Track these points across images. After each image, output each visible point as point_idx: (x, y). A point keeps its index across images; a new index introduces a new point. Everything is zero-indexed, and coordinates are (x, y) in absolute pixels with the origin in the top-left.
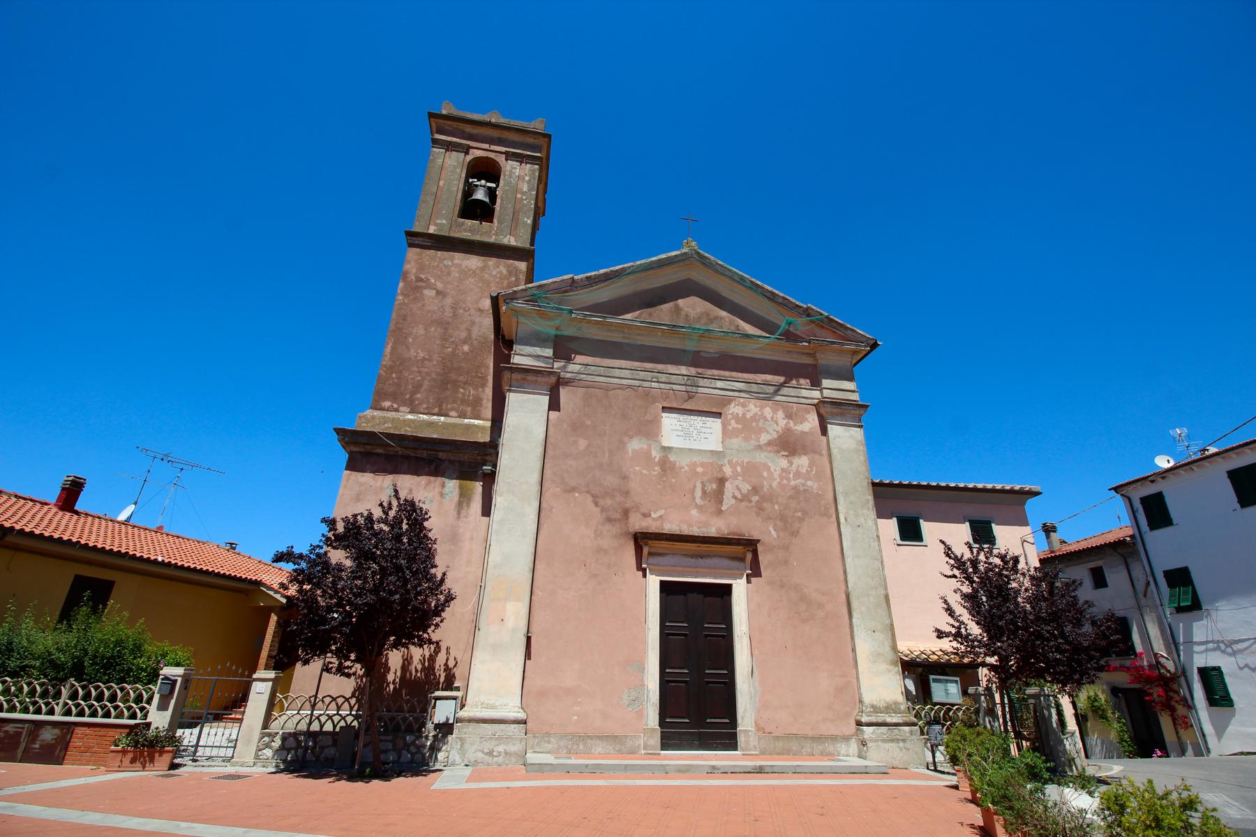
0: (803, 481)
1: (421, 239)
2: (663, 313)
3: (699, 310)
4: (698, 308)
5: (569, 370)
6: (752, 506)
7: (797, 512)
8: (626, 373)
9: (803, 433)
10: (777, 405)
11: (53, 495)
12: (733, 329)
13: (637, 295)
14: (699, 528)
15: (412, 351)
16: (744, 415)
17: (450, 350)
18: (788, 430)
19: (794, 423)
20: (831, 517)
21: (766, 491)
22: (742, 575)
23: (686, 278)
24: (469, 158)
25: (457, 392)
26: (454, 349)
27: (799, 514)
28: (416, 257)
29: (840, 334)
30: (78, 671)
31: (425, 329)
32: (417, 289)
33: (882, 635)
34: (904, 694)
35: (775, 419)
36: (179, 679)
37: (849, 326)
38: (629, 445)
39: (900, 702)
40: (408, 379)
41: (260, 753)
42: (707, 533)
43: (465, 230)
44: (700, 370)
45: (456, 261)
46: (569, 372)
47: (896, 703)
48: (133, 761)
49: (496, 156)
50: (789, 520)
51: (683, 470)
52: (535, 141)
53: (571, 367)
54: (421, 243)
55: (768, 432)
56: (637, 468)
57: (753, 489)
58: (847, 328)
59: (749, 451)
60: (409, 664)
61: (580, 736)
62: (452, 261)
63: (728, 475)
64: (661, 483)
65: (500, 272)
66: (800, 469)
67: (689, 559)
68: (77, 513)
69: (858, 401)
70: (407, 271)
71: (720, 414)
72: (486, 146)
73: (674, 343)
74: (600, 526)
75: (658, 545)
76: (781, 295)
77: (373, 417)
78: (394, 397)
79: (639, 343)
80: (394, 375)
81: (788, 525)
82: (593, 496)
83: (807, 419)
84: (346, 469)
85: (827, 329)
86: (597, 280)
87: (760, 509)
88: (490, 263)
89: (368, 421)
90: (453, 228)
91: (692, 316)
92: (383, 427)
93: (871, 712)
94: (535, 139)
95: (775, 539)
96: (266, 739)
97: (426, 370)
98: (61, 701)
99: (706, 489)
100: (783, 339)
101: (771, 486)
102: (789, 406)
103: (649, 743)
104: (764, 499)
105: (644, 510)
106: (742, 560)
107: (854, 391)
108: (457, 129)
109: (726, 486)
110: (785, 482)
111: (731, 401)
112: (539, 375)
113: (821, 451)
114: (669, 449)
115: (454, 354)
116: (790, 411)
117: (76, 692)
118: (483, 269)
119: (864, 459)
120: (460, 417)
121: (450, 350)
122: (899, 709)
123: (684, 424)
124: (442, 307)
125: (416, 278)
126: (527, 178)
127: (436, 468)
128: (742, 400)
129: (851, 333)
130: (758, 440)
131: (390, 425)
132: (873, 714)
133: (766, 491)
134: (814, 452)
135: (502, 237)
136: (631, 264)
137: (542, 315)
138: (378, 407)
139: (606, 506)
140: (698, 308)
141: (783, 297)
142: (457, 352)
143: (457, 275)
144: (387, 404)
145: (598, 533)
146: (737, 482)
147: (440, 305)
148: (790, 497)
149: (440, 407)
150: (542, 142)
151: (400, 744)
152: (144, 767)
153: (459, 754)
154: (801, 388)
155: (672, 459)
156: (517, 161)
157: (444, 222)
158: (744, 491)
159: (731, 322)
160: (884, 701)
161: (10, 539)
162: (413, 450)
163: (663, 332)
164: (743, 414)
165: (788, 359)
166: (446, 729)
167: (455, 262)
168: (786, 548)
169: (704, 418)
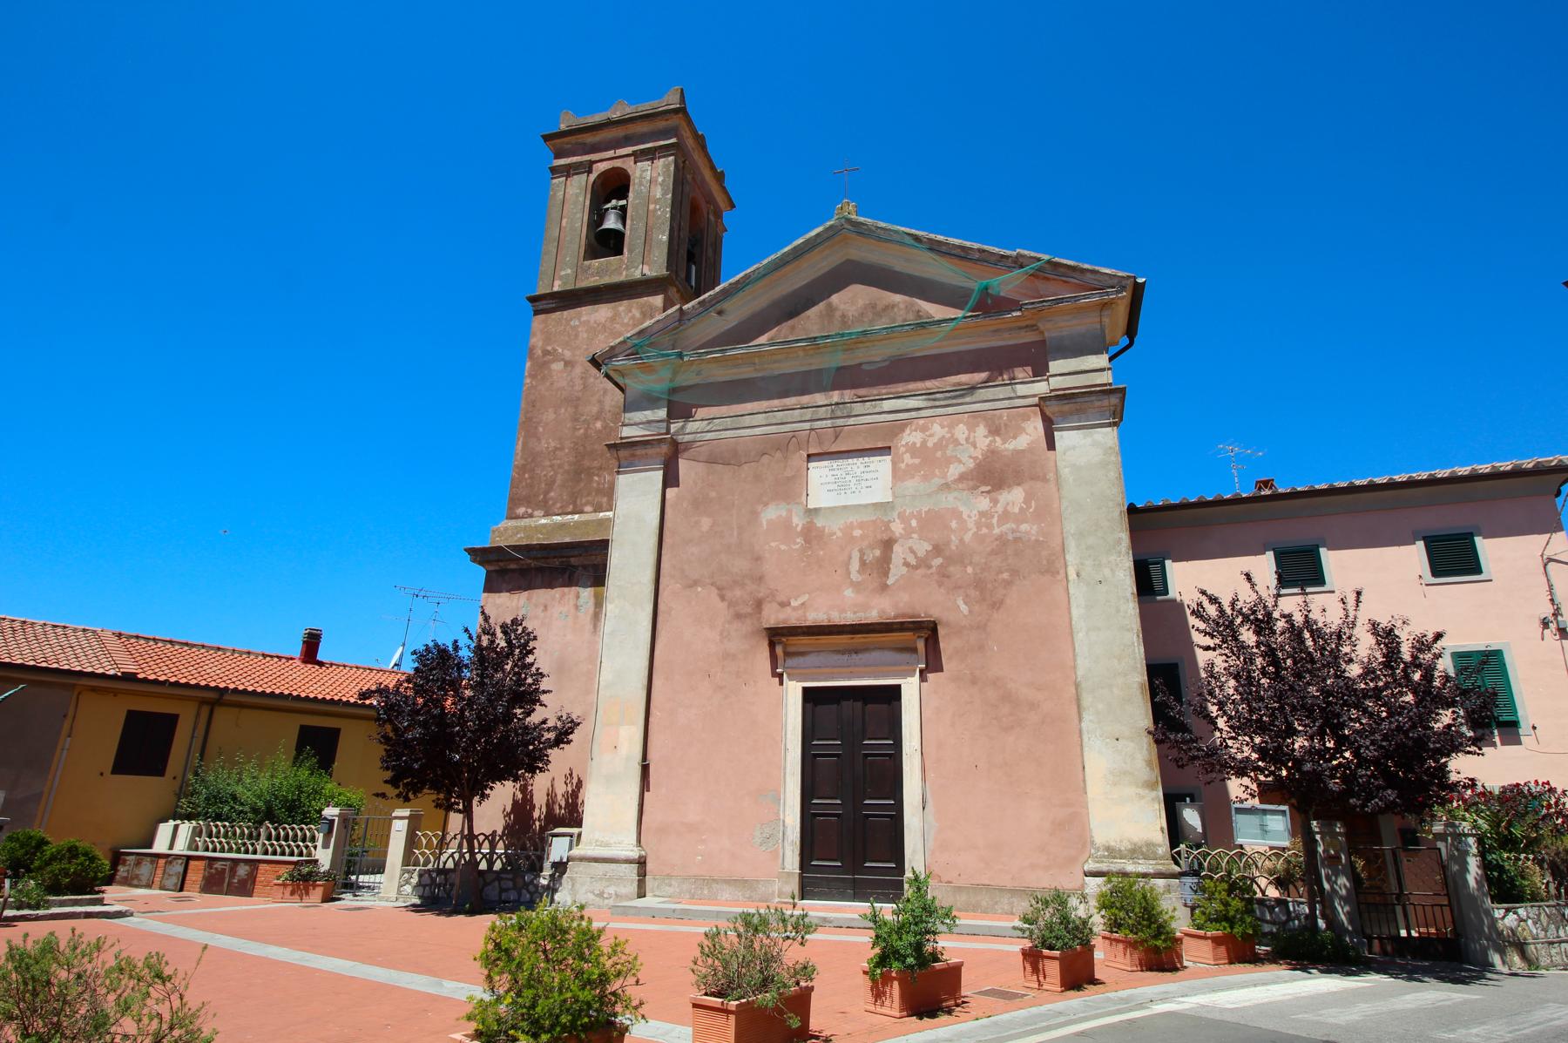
0: (1014, 526)
1: (544, 302)
2: (811, 321)
3: (861, 303)
4: (860, 300)
5: (687, 431)
6: (932, 574)
7: (1002, 573)
8: (760, 419)
9: (1018, 453)
10: (975, 417)
11: (296, 650)
12: (911, 318)
13: (775, 304)
14: (855, 613)
15: (543, 441)
16: (924, 443)
17: (582, 431)
18: (993, 452)
19: (1002, 440)
20: (1058, 573)
21: (954, 548)
22: (915, 671)
23: (844, 259)
24: (593, 177)
25: (591, 481)
26: (586, 430)
27: (1006, 576)
28: (541, 326)
29: (1075, 284)
30: (270, 815)
31: (555, 413)
32: (545, 365)
33: (1132, 744)
34: (1166, 831)
35: (971, 440)
36: (337, 819)
37: (1086, 266)
38: (763, 515)
39: (1157, 842)
40: (540, 477)
41: (402, 889)
42: (866, 618)
43: (592, 275)
44: (862, 392)
45: (584, 318)
46: (688, 434)
47: (1149, 844)
48: (292, 893)
49: (624, 162)
50: (989, 586)
51: (835, 537)
52: (669, 122)
53: (692, 426)
54: (545, 306)
55: (960, 462)
56: (773, 544)
57: (934, 548)
58: (1084, 271)
59: (929, 495)
60: (554, 803)
61: (704, 880)
62: (579, 320)
63: (897, 534)
64: (805, 559)
65: (633, 317)
66: (1009, 508)
67: (840, 657)
68: (321, 664)
69: (1110, 384)
70: (533, 346)
71: (890, 448)
72: (610, 154)
73: (816, 363)
74: (727, 626)
75: (799, 642)
76: (976, 246)
77: (506, 529)
78: (527, 501)
79: (776, 373)
80: (527, 476)
81: (987, 593)
82: (718, 589)
83: (1024, 429)
84: (484, 591)
85: (1054, 279)
86: (713, 302)
87: (943, 575)
88: (621, 309)
89: (501, 534)
90: (579, 277)
91: (850, 314)
92: (516, 538)
93: (1104, 856)
94: (667, 120)
95: (965, 616)
96: (406, 875)
97: (558, 462)
98: (260, 842)
99: (865, 558)
100: (979, 315)
101: (961, 540)
102: (995, 415)
103: (784, 890)
104: (950, 560)
105: (781, 598)
106: (914, 650)
107: (1102, 370)
108: (576, 144)
109: (894, 550)
110: (984, 530)
111: (905, 426)
112: (648, 446)
113: (1045, 475)
114: (816, 510)
115: (586, 436)
116: (997, 422)
117: (270, 833)
118: (613, 319)
119: (1117, 475)
120: (595, 511)
121: (582, 431)
122: (1155, 853)
123: (839, 473)
124: (571, 380)
125: (542, 352)
126: (660, 179)
127: (569, 578)
128: (921, 422)
129: (1092, 276)
130: (944, 476)
131: (523, 535)
132: (1105, 860)
133: (954, 548)
134: (1034, 478)
135: (633, 270)
136: (755, 267)
137: (648, 369)
138: (514, 516)
139: (734, 599)
140: (860, 300)
141: (979, 250)
142: (589, 432)
143: (585, 335)
144: (521, 511)
145: (725, 634)
146: (910, 543)
147: (569, 379)
148: (994, 553)
149: (574, 503)
150: (675, 121)
151: (520, 881)
152: (301, 899)
153: (570, 894)
154: (1016, 384)
155: (819, 525)
156: (648, 160)
157: (569, 271)
158: (921, 554)
159: (908, 308)
160: (1129, 841)
161: (227, 697)
162: (543, 560)
163: (804, 350)
164: (922, 442)
165: (995, 342)
166: (561, 867)
167: (582, 319)
168: (982, 627)
169: (866, 459)
